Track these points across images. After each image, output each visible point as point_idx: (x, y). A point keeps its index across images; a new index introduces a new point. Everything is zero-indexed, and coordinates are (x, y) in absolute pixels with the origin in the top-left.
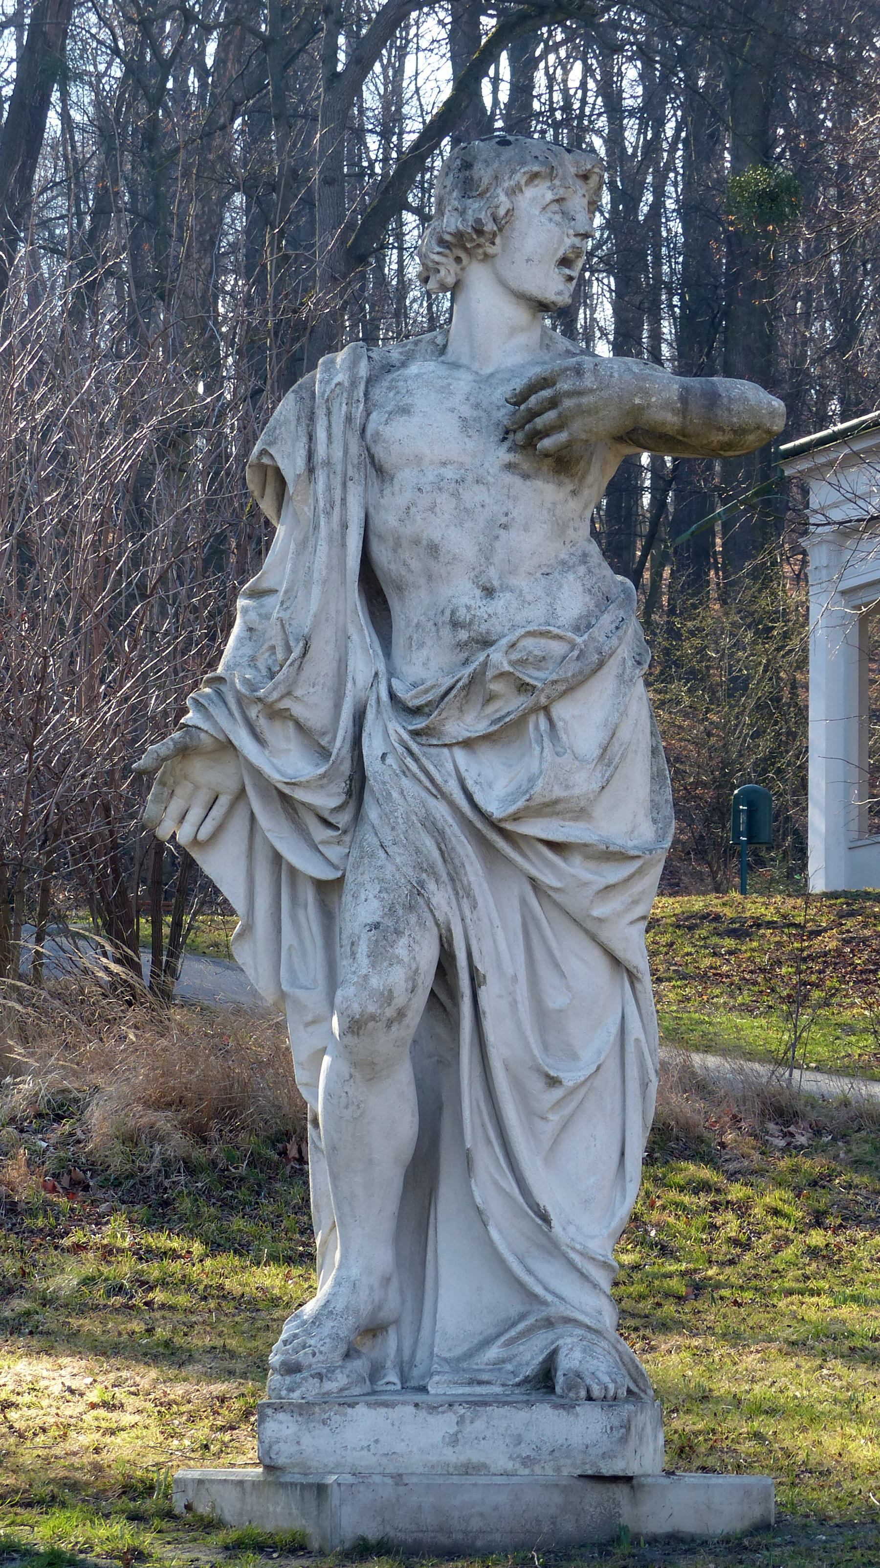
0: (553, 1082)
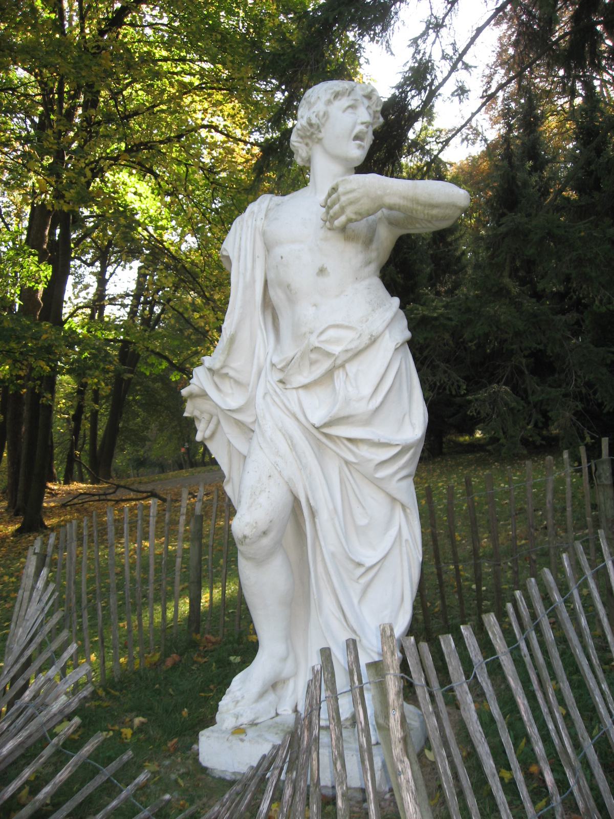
0: (359, 565)
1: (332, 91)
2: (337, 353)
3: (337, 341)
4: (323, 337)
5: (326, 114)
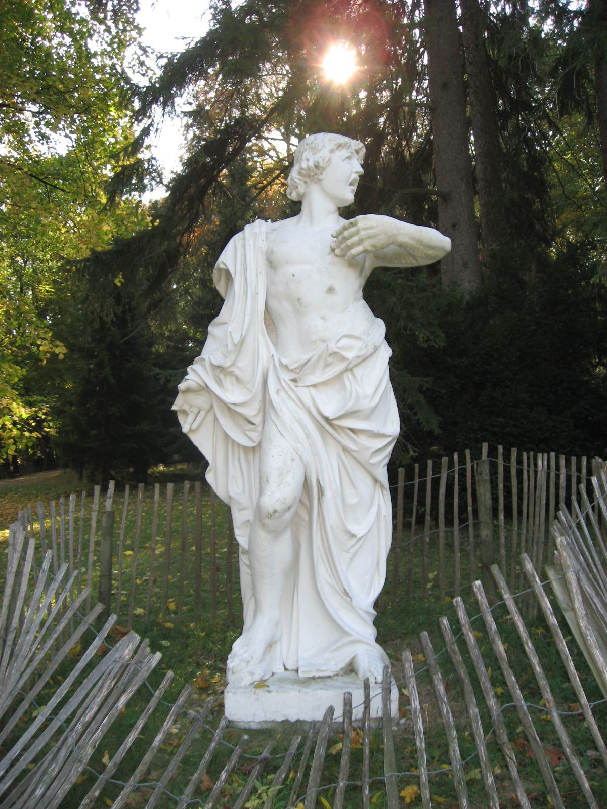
0: (353, 536)
1: (335, 142)
2: (350, 359)
3: (349, 348)
4: (340, 344)
5: (330, 160)
